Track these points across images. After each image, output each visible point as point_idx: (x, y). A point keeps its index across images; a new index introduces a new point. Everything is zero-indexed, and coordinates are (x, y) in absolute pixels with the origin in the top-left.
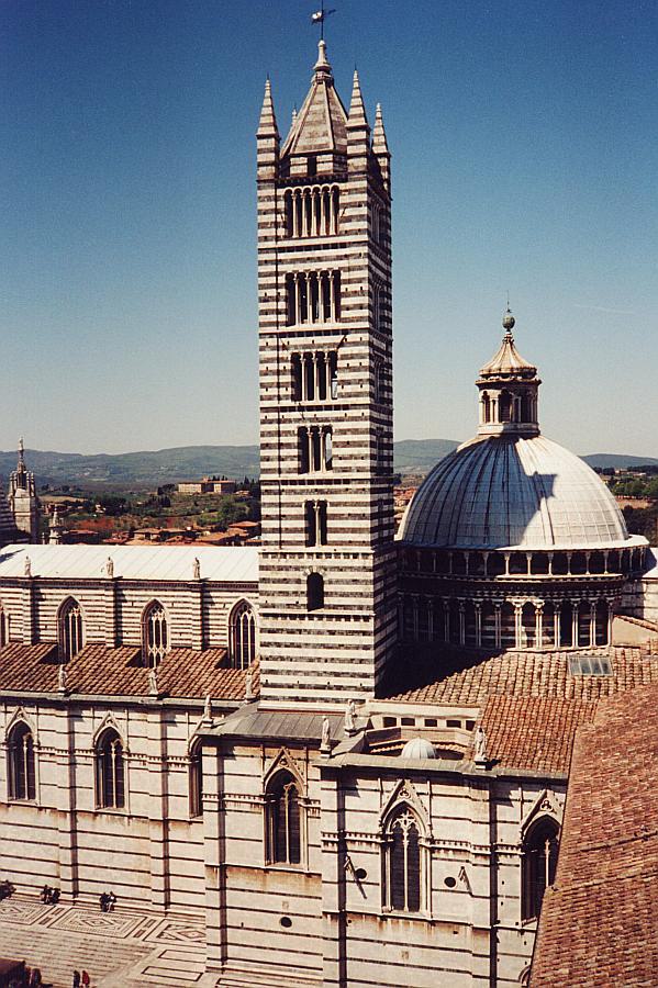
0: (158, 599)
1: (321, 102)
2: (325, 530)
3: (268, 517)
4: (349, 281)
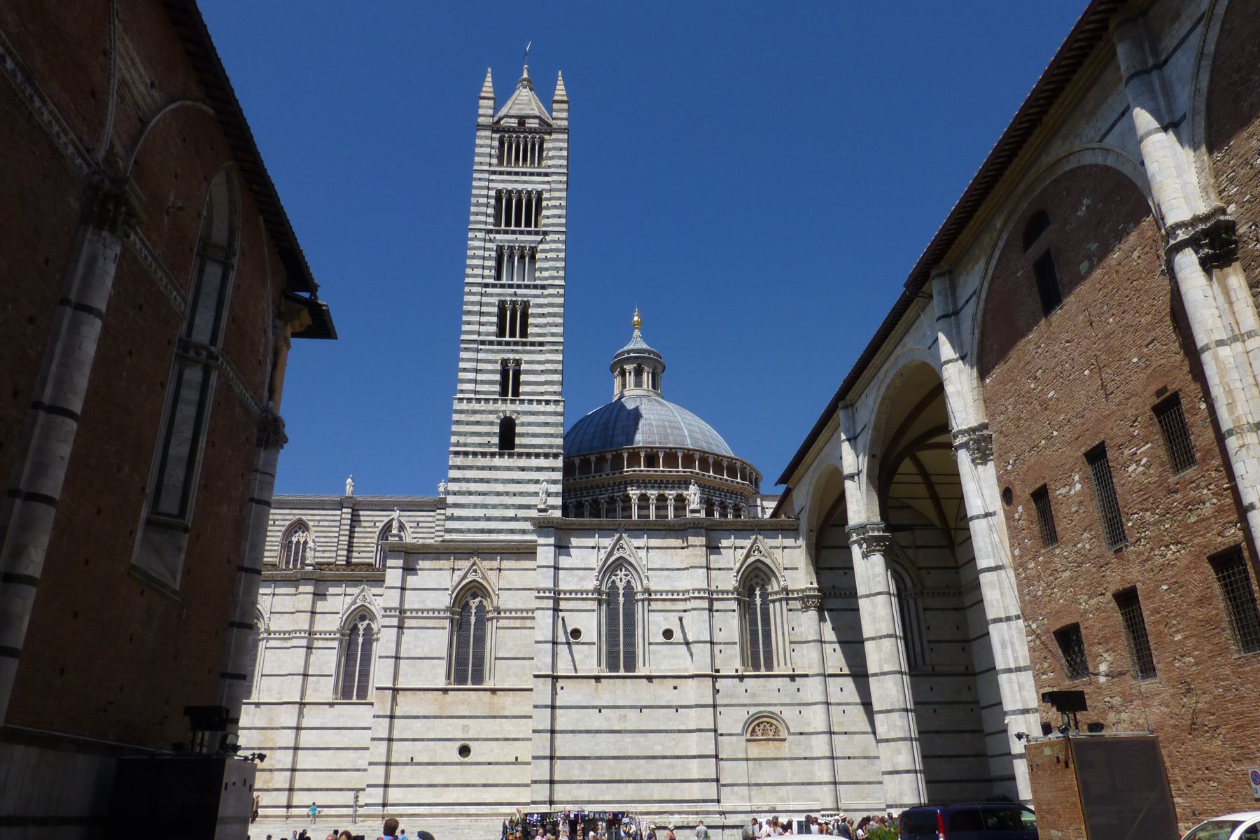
0: (304, 518)
2: (517, 384)
3: (465, 370)
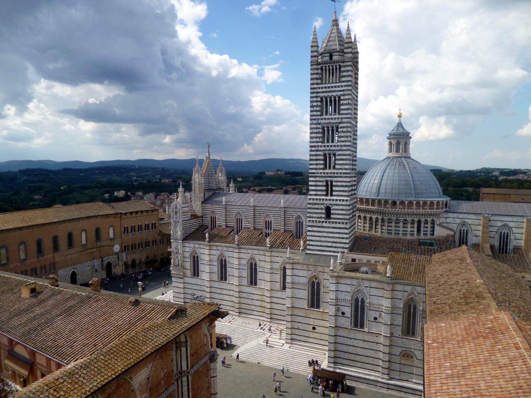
1: (334, 33)
2: (332, 191)
3: (312, 186)
4: (344, 100)
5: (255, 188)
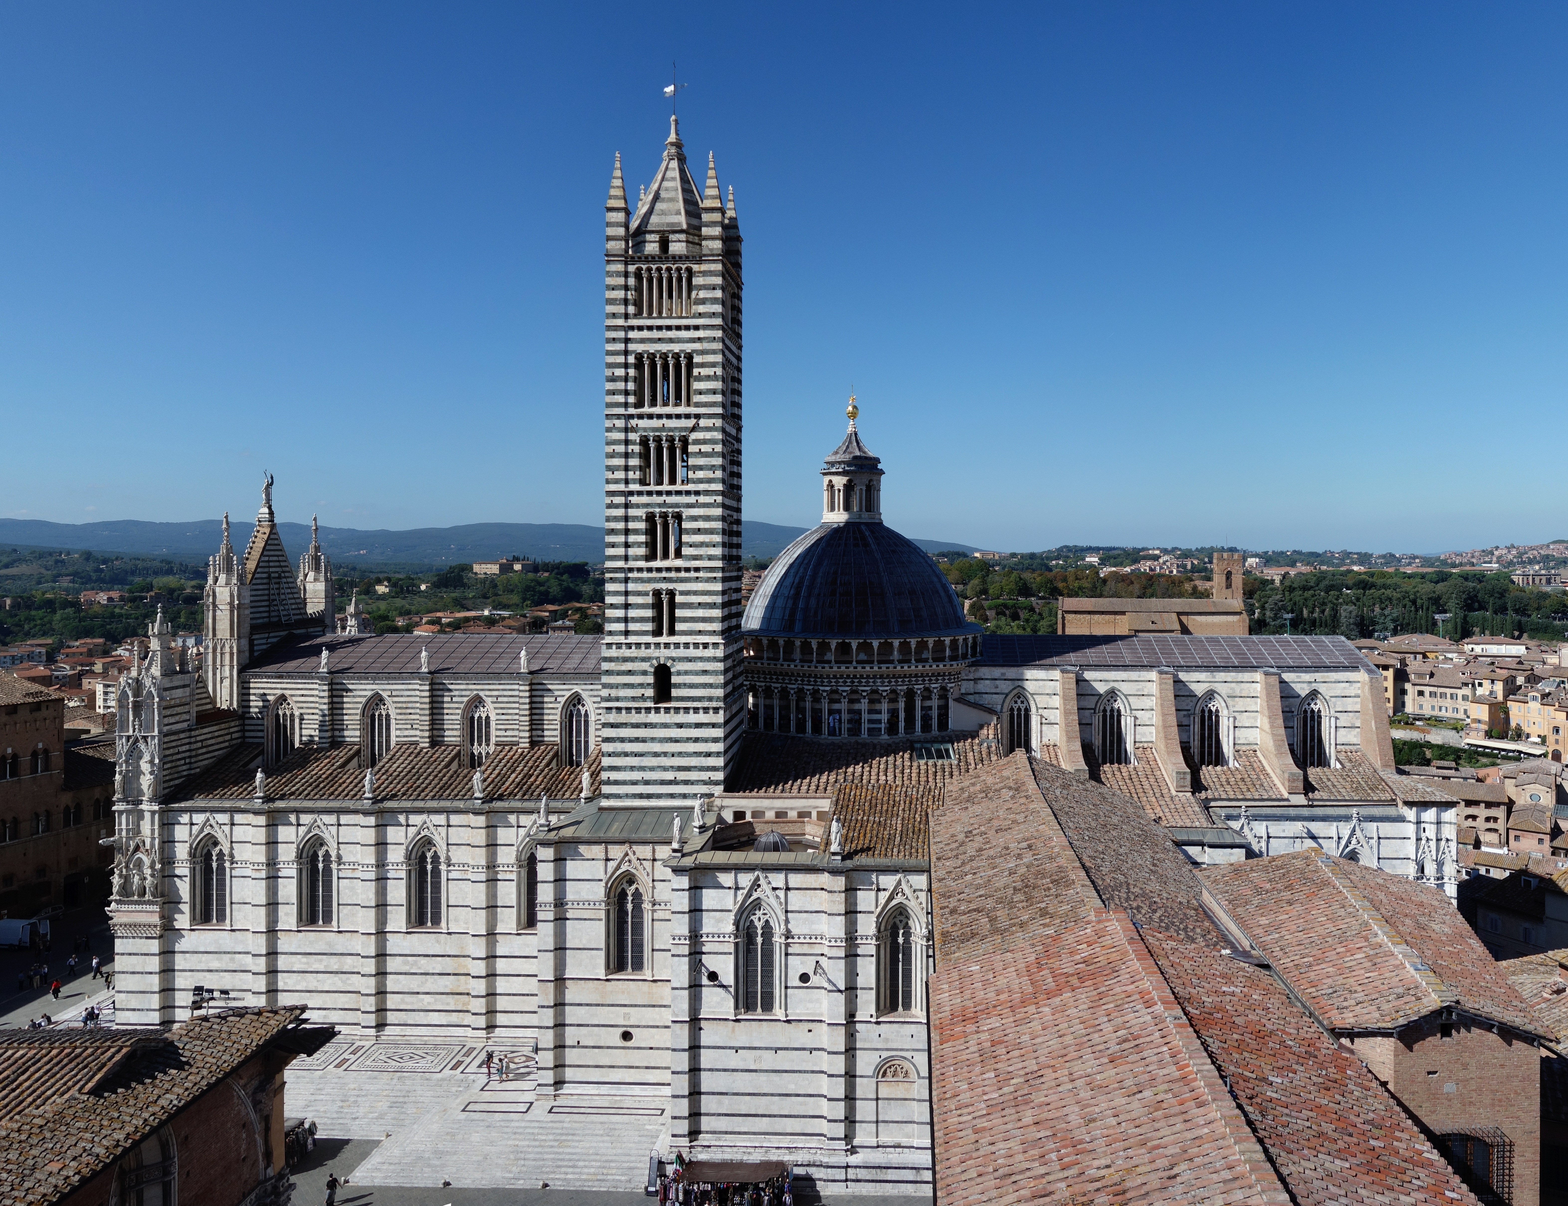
1: (673, 179)
2: (673, 620)
3: (612, 606)
4: (702, 365)
5: (439, 614)
